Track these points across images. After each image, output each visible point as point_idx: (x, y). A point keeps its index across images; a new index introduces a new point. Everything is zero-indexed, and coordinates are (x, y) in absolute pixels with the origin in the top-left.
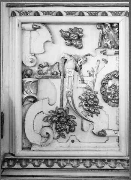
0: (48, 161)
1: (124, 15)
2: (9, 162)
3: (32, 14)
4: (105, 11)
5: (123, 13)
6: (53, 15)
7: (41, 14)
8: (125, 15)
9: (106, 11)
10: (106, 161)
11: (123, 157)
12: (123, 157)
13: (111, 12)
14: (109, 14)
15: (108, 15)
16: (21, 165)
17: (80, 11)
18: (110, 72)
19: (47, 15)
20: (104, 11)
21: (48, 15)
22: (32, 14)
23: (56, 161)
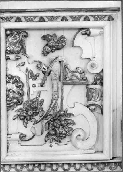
0: (40, 165)
1: (61, 20)
2: (40, 167)
3: (14, 20)
4: (42, 17)
5: (37, 18)
6: (81, 20)
7: (69, 19)
8: (108, 20)
9: (65, 16)
10: (95, 164)
11: (107, 160)
12: (107, 160)
13: (94, 17)
14: (92, 19)
15: (68, 21)
16: (110, 168)
17: (41, 16)
18: (5, 95)
19: (17, 22)
20: (18, 17)
21: (100, 20)
22: (14, 20)
23: (83, 165)
